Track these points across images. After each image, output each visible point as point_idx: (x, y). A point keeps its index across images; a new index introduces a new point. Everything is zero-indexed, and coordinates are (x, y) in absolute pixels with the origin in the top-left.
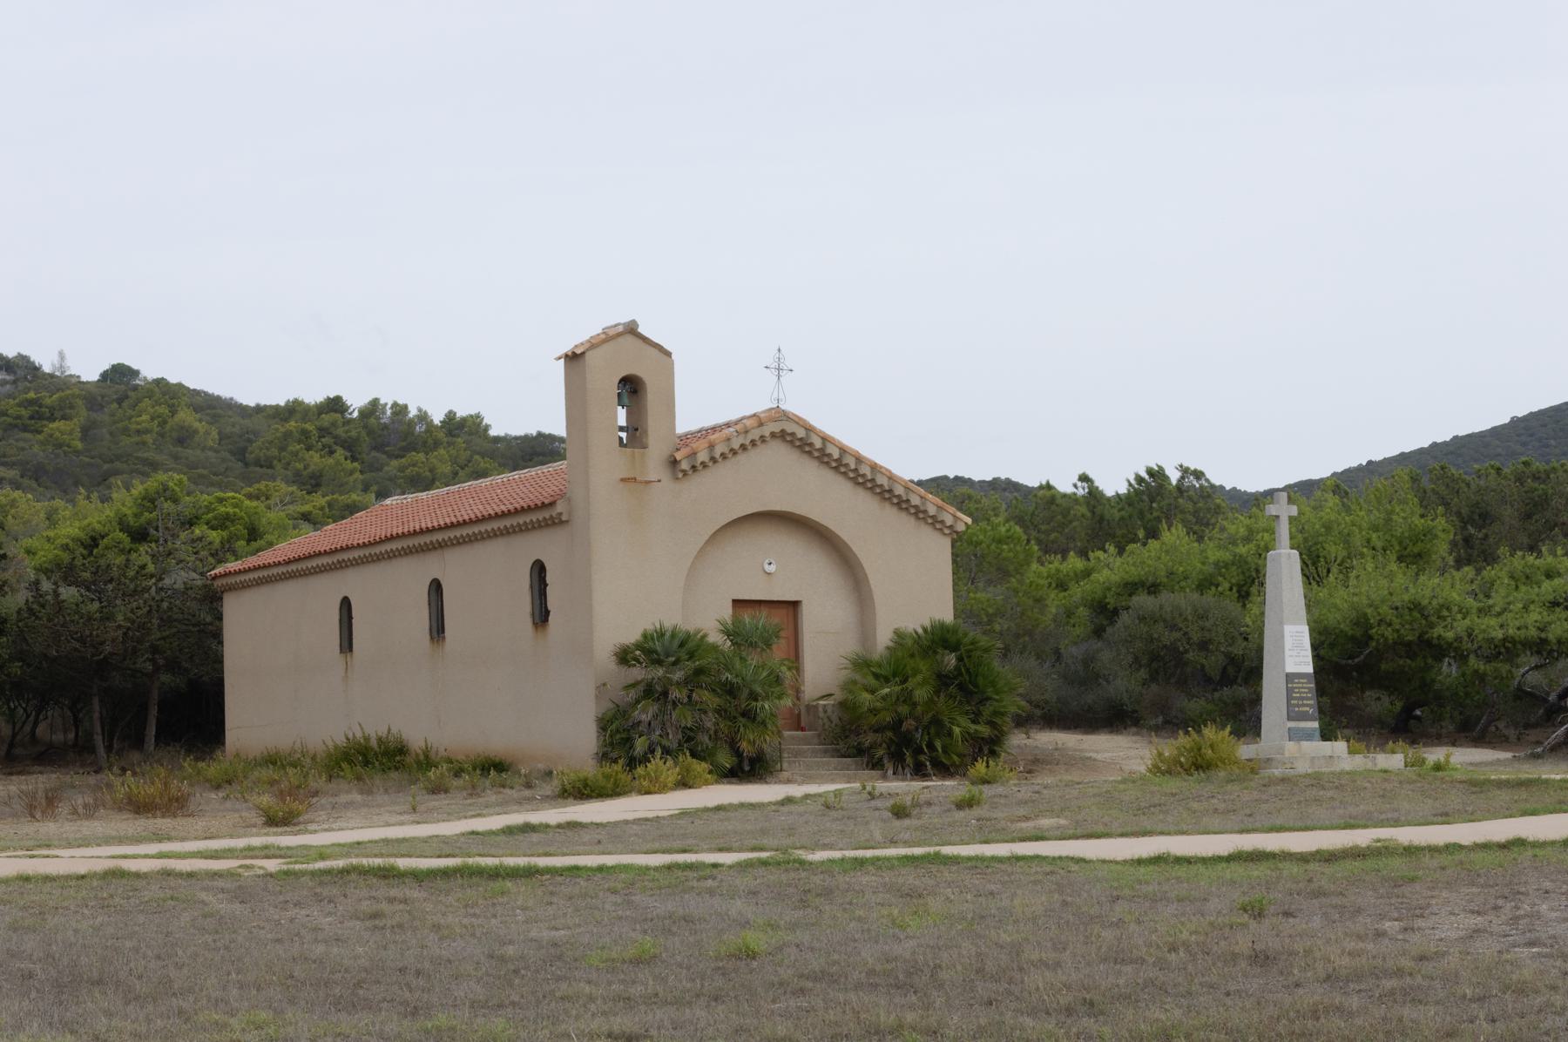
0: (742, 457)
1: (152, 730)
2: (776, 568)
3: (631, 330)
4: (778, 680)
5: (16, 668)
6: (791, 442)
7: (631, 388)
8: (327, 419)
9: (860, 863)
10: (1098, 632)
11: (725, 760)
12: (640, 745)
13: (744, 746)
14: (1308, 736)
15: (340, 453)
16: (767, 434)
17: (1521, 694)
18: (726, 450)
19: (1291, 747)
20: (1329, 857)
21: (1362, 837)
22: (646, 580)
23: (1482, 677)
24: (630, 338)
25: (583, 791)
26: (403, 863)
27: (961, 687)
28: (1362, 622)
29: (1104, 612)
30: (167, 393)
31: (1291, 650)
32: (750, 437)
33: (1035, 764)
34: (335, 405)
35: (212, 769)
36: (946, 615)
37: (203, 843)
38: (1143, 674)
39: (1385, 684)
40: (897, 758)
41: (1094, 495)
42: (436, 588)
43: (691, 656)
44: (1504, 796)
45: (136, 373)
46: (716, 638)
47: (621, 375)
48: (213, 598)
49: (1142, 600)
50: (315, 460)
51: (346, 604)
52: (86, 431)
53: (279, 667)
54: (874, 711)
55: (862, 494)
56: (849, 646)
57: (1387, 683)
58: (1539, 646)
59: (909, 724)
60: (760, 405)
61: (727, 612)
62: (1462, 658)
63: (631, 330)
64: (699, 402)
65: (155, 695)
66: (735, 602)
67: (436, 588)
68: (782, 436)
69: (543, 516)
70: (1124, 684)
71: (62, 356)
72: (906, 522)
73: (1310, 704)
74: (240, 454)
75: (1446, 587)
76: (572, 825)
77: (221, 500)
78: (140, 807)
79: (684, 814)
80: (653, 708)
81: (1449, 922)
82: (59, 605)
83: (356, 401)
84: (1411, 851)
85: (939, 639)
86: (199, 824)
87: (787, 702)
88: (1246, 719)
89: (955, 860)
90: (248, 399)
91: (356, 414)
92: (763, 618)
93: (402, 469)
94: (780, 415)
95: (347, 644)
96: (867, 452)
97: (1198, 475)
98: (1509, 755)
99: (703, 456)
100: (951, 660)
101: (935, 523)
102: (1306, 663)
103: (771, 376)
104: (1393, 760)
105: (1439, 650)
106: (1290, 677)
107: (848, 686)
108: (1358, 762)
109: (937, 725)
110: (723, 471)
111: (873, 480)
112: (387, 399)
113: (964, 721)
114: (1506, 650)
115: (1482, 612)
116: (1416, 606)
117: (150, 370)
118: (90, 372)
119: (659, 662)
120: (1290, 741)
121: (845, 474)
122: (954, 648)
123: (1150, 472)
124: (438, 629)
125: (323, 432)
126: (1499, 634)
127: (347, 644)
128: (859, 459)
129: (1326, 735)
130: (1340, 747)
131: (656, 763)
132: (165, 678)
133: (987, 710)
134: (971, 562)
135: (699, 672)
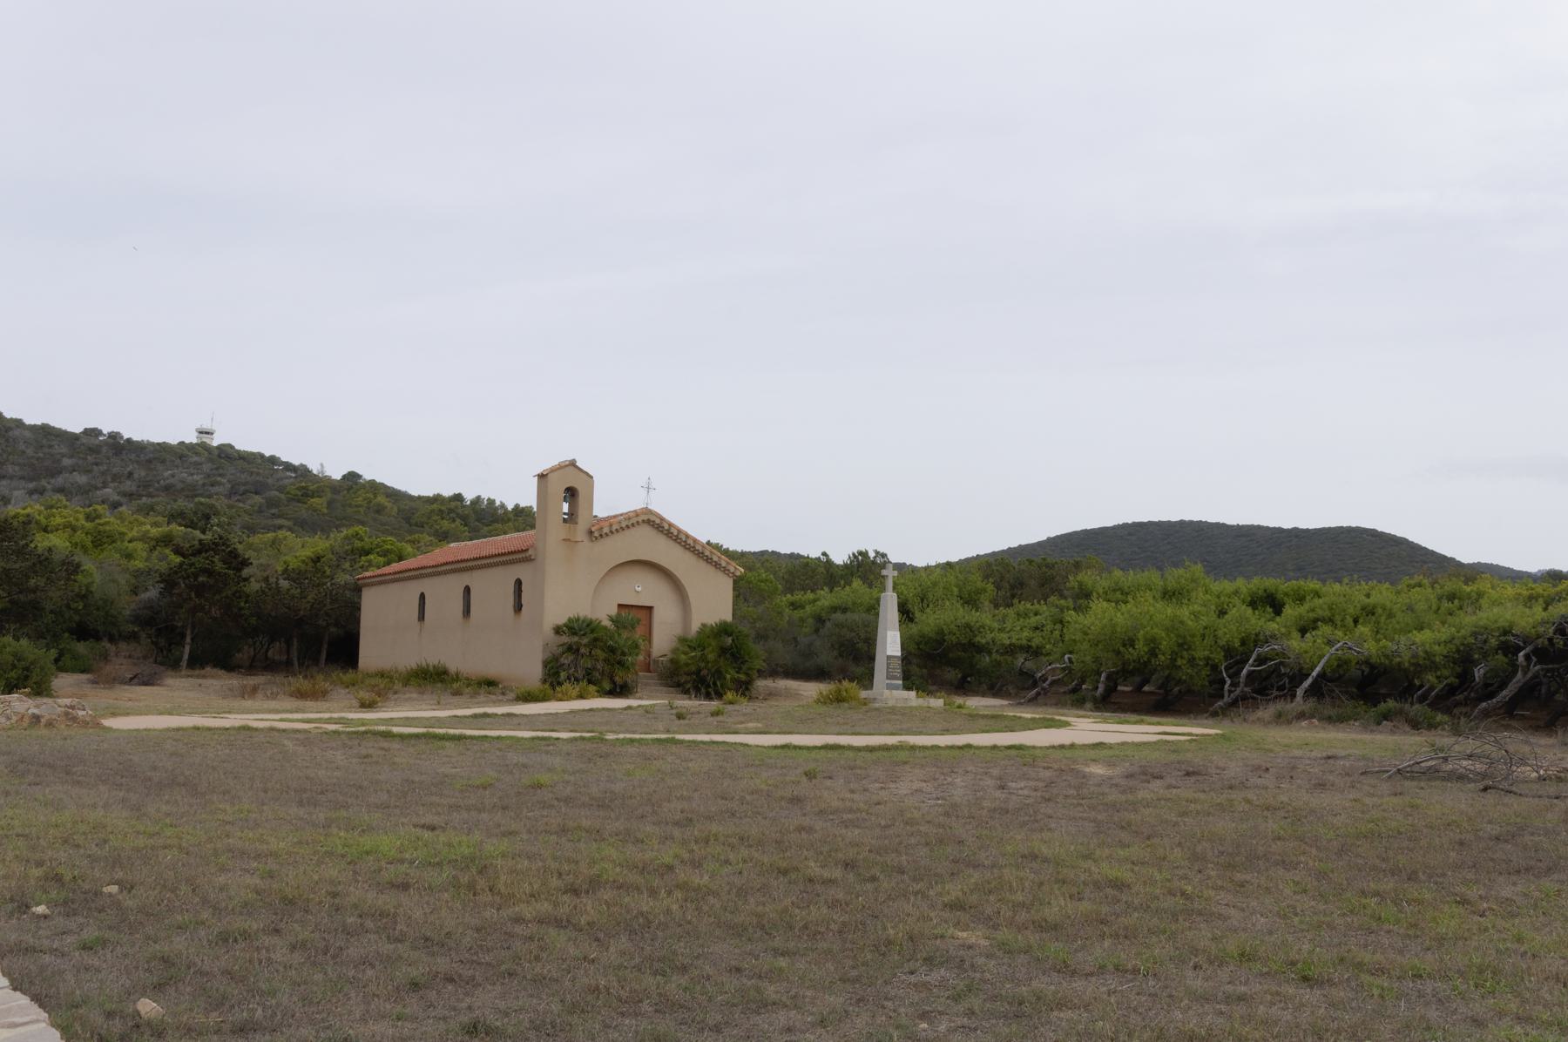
0: (627, 532)
1: (324, 656)
2: (641, 589)
3: (573, 464)
4: (637, 646)
5: (253, 621)
7: (571, 493)
8: (453, 504)
9: (632, 741)
10: (817, 631)
11: (607, 686)
12: (563, 675)
13: (617, 679)
14: (896, 688)
15: (458, 521)
17: (1022, 673)
19: (887, 692)
20: (871, 749)
21: (891, 740)
22: (572, 592)
23: (999, 663)
25: (528, 698)
26: (395, 730)
27: (733, 655)
28: (941, 632)
29: (820, 620)
30: (375, 487)
31: (891, 643)
33: (771, 695)
34: (458, 498)
35: (349, 676)
36: (729, 618)
37: (332, 713)
38: (835, 653)
39: (945, 664)
40: (697, 690)
41: (829, 563)
42: (467, 590)
43: (592, 631)
44: (982, 722)
45: (360, 477)
46: (606, 623)
47: (568, 485)
48: (358, 589)
49: (839, 616)
50: (446, 525)
51: (422, 596)
52: (330, 504)
53: (387, 627)
54: (687, 665)
56: (678, 631)
57: (954, 664)
58: (1027, 649)
59: (704, 672)
61: (614, 611)
62: (990, 653)
63: (573, 464)
64: (607, 502)
65: (327, 638)
66: (620, 606)
67: (467, 590)
68: (648, 522)
69: (521, 556)
70: (825, 657)
72: (710, 569)
73: (898, 672)
74: (408, 520)
75: (984, 617)
76: (510, 715)
78: (301, 695)
79: (572, 712)
80: (571, 657)
81: (908, 787)
82: (278, 589)
83: (469, 496)
84: (913, 748)
85: (723, 630)
86: (326, 705)
87: (641, 657)
88: (867, 680)
89: (682, 742)
90: (415, 492)
92: (633, 614)
94: (647, 511)
95: (422, 617)
96: (692, 533)
97: (884, 555)
98: (1005, 702)
99: (606, 530)
100: (729, 640)
101: (725, 570)
104: (937, 703)
105: (980, 649)
106: (889, 657)
107: (675, 651)
108: (921, 702)
109: (719, 674)
110: (617, 537)
112: (485, 496)
113: (732, 672)
114: (1011, 650)
115: (1001, 630)
116: (968, 626)
117: (368, 475)
118: (336, 474)
119: (575, 634)
120: (887, 690)
122: (730, 634)
123: (860, 553)
124: (467, 611)
125: (451, 511)
126: (1007, 642)
127: (422, 617)
128: (687, 536)
129: (907, 688)
130: (913, 693)
131: (566, 686)
132: (333, 629)
133: (744, 667)
134: (743, 591)
135: (596, 640)
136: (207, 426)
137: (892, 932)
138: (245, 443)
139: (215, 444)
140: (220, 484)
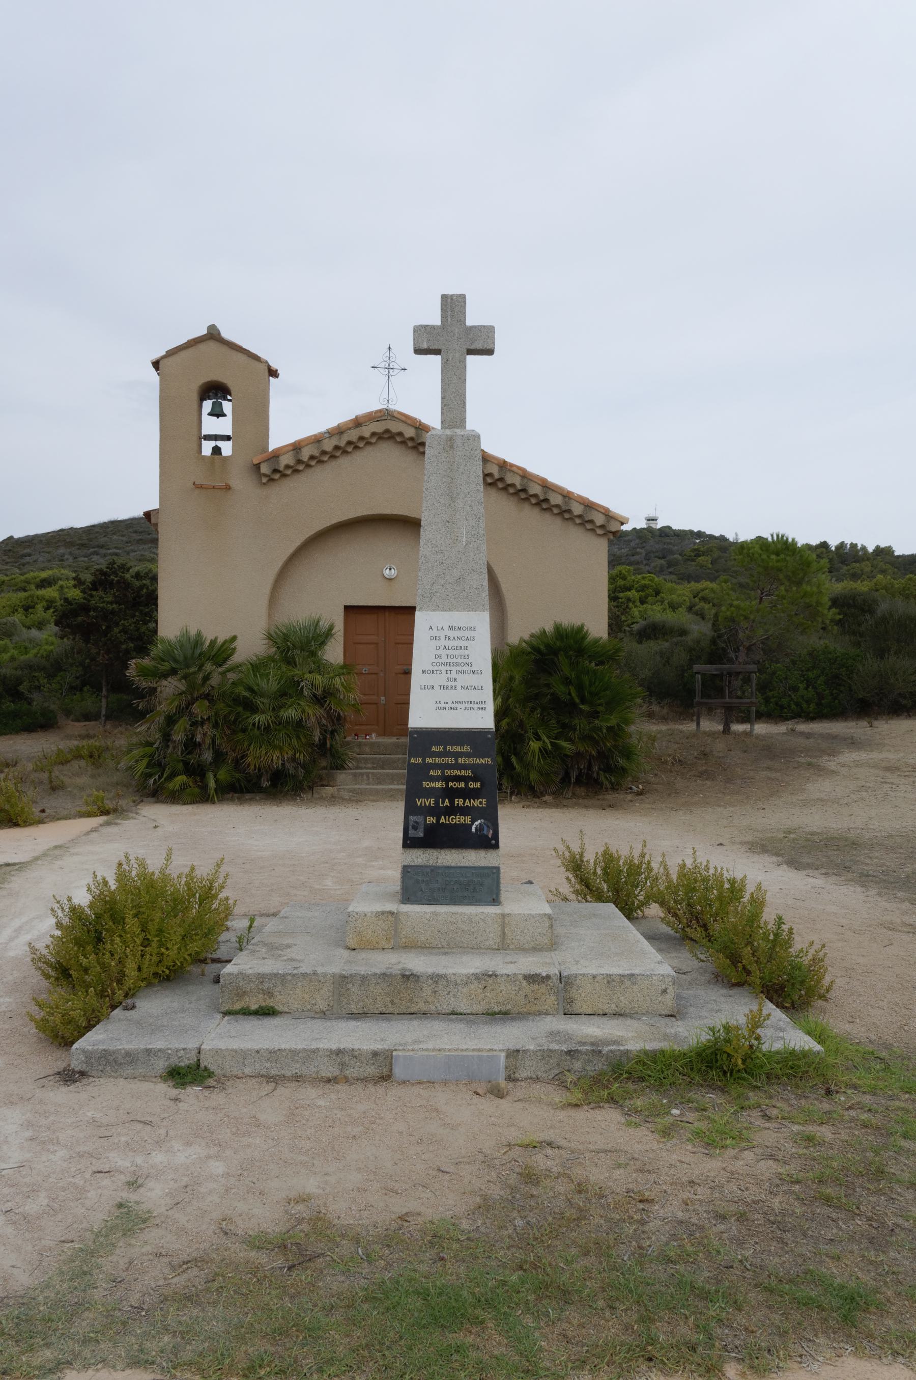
6: (403, 443)
16: (367, 434)
18: (316, 453)
24: (212, 345)
32: (345, 438)
47: (211, 376)
60: (374, 405)
63: (213, 335)
66: (348, 609)
68: (388, 436)
71: (737, 535)
72: (552, 525)
77: (644, 578)
83: (833, 543)
91: (833, 549)
93: (848, 570)
102: (471, 706)
103: (379, 377)
111: (501, 479)
112: (848, 541)
136: (652, 515)
137: (890, 1092)
138: (679, 524)
139: (659, 527)
140: (638, 553)
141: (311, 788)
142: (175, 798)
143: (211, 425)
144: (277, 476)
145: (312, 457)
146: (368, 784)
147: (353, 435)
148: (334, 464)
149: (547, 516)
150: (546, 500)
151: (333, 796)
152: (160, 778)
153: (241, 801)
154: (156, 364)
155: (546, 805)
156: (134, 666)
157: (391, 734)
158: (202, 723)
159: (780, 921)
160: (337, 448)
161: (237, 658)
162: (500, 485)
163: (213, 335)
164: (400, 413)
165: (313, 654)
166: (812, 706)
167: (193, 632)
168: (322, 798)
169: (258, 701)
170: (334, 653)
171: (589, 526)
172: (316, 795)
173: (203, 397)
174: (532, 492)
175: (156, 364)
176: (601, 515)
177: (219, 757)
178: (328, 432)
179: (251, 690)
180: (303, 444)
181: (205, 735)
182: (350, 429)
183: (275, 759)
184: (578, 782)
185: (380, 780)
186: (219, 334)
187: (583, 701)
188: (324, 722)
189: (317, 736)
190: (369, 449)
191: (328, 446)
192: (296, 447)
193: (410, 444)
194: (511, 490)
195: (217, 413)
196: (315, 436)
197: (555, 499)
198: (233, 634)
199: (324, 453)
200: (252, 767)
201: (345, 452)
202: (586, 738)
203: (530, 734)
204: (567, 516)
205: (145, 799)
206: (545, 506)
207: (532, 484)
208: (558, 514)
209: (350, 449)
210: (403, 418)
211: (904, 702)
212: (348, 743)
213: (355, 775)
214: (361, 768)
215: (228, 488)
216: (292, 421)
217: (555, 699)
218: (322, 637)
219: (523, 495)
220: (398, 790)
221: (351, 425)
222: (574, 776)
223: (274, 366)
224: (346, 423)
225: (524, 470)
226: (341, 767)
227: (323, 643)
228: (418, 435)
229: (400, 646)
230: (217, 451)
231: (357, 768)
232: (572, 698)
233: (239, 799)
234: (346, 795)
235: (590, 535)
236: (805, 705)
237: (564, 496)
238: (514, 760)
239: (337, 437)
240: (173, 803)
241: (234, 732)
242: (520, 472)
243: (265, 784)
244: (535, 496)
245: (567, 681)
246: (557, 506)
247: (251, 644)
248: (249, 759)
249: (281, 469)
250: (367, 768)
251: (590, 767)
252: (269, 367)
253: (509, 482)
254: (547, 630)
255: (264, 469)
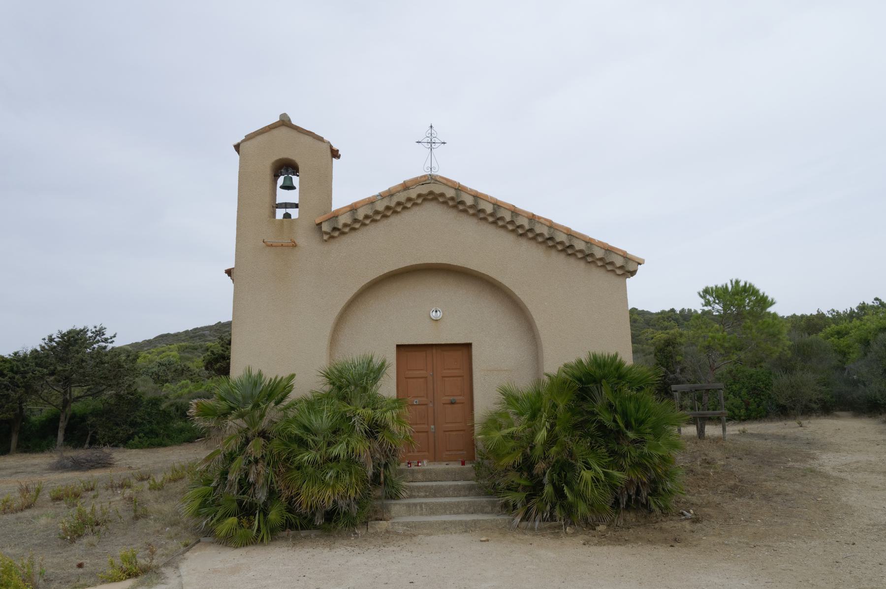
2: (437, 315)
6: (445, 203)
16: (414, 196)
18: (370, 213)
24: (284, 130)
32: (395, 200)
34: (673, 310)
50: (666, 324)
55: (524, 244)
59: (540, 466)
63: (285, 122)
66: (398, 346)
68: (431, 197)
83: (678, 310)
87: (608, 507)
94: (430, 179)
96: (559, 219)
103: (424, 149)
109: (564, 470)
111: (531, 230)
112: (686, 308)
121: (504, 227)
128: (515, 212)
141: (366, 523)
142: (229, 541)
143: (283, 196)
144: (336, 234)
145: (367, 217)
146: (421, 515)
147: (402, 197)
148: (385, 222)
149: (572, 260)
150: (571, 246)
151: (387, 532)
152: (212, 519)
153: (296, 542)
154: (237, 147)
155: (604, 539)
156: (195, 406)
157: (441, 460)
158: (256, 461)
159: (495, 404)
160: (388, 208)
161: (293, 396)
162: (530, 235)
163: (285, 122)
164: (441, 177)
165: (365, 389)
166: (743, 412)
167: (255, 373)
168: (376, 534)
169: (309, 439)
170: (387, 387)
171: (609, 268)
172: (371, 531)
173: (276, 176)
174: (558, 239)
175: (237, 147)
176: (619, 257)
177: (273, 494)
178: (380, 195)
179: (306, 429)
180: (359, 205)
181: (258, 474)
182: (399, 192)
183: (327, 497)
184: (628, 507)
185: (433, 510)
186: (290, 120)
187: (628, 426)
188: (378, 456)
189: (370, 471)
190: (416, 209)
191: (380, 206)
192: (353, 209)
193: (451, 203)
194: (540, 239)
195: (288, 187)
196: (369, 198)
197: (579, 245)
198: (292, 373)
199: (377, 212)
200: (304, 506)
201: (395, 212)
202: (636, 465)
203: (580, 464)
204: (589, 259)
205: (202, 539)
206: (570, 251)
207: (558, 233)
208: (581, 258)
209: (399, 209)
210: (445, 182)
211: (814, 406)
212: (401, 472)
213: (408, 506)
214: (415, 497)
215: (295, 245)
216: (349, 188)
217: (602, 426)
218: (374, 373)
219: (550, 243)
220: (451, 522)
221: (399, 189)
222: (624, 500)
223: (335, 147)
224: (395, 187)
225: (550, 222)
226: (395, 496)
227: (376, 379)
228: (457, 195)
229: (447, 379)
230: (287, 216)
231: (411, 497)
232: (618, 426)
233: (294, 537)
234: (400, 529)
235: (611, 276)
236: (737, 411)
237: (587, 243)
238: (566, 490)
239: (388, 199)
240: (226, 546)
241: (288, 470)
242: (548, 224)
243: (319, 521)
244: (561, 243)
245: (610, 407)
246: (581, 251)
247: (309, 382)
248: (302, 498)
249: (340, 227)
250: (420, 497)
251: (638, 492)
252: (331, 147)
253: (538, 232)
254: (583, 360)
255: (326, 227)
